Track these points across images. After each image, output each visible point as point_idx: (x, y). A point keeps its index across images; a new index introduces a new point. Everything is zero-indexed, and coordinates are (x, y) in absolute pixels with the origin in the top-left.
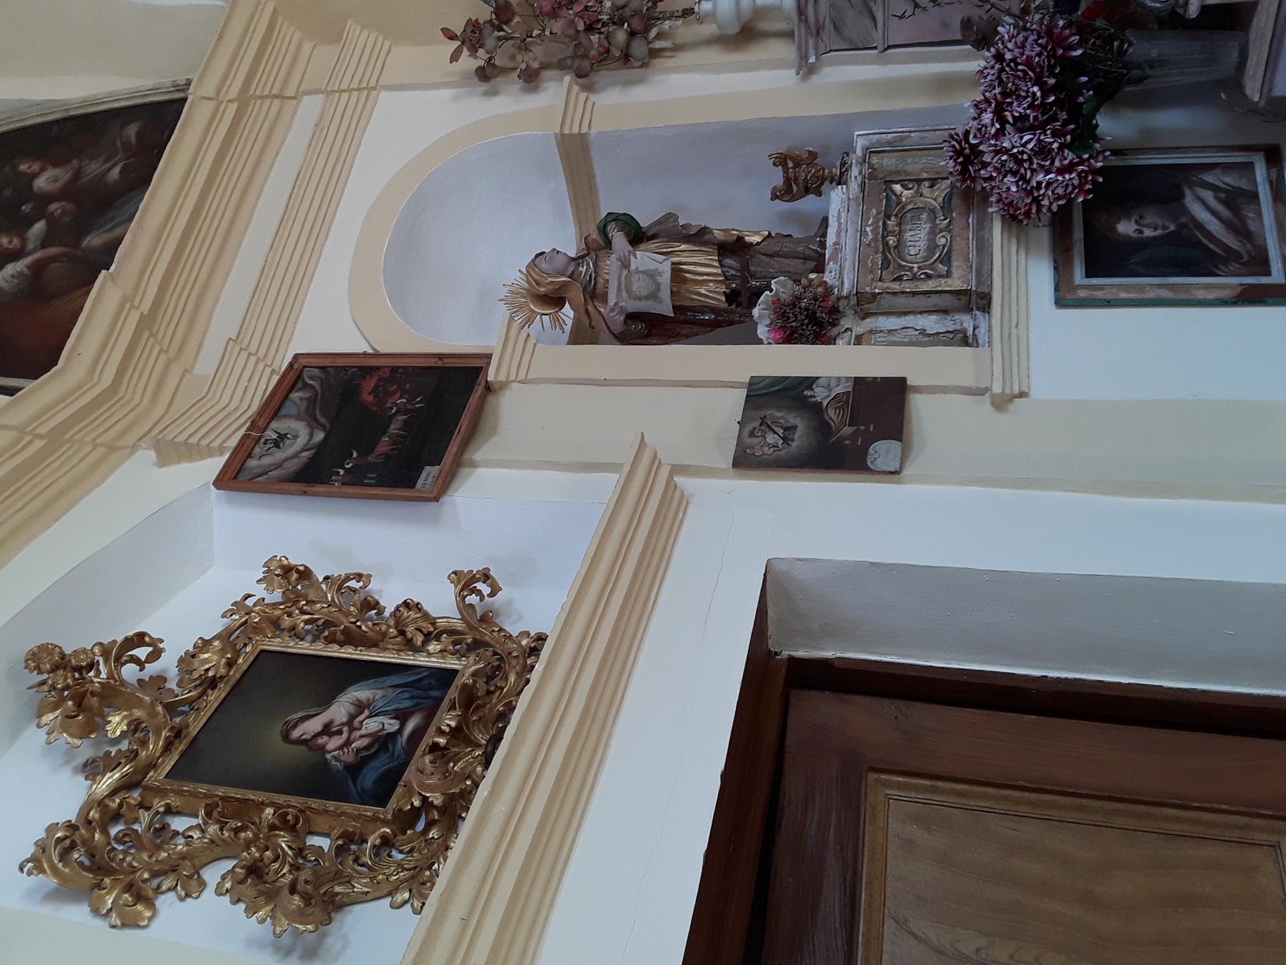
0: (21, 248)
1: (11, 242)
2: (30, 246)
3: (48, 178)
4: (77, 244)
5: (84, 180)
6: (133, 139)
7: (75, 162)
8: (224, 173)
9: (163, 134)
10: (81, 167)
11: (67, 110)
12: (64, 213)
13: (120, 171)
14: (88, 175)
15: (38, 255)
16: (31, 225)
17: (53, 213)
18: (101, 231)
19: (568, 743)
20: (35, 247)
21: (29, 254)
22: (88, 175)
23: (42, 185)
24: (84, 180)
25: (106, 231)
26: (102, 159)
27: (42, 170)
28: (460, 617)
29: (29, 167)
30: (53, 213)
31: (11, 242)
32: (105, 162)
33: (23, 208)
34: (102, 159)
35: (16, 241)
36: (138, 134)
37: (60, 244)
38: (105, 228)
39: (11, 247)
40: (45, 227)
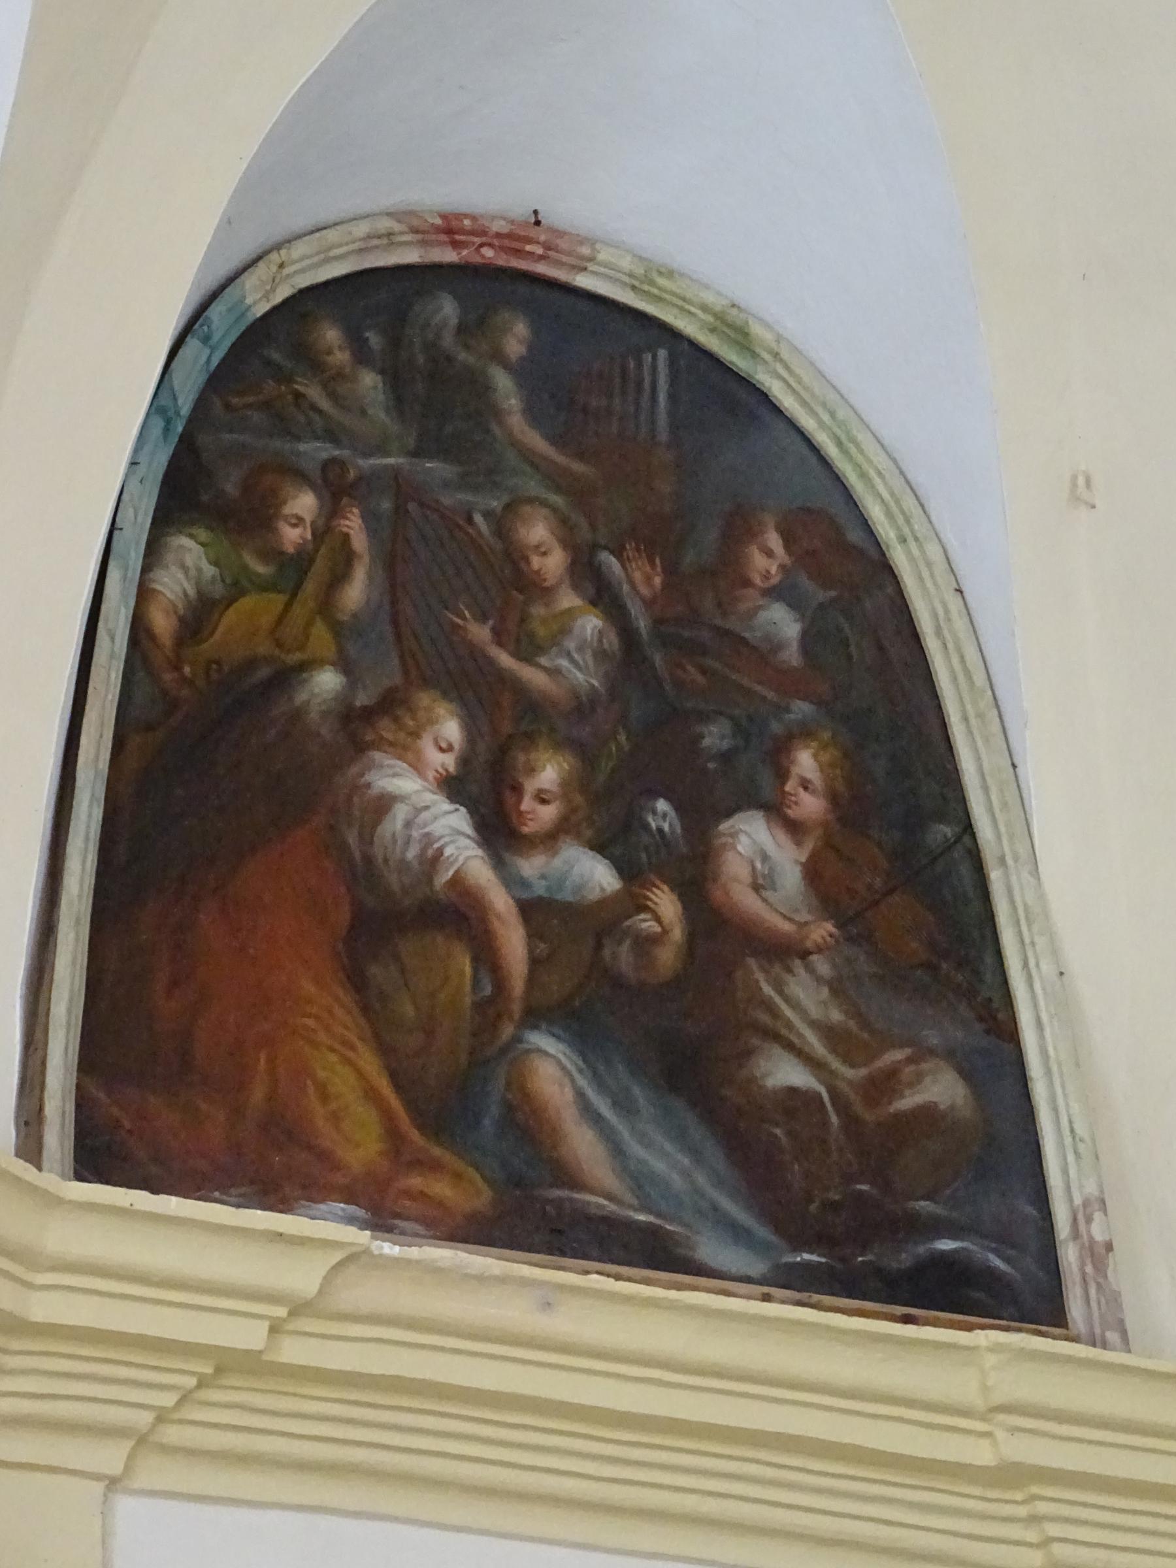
0: (524, 837)
1: (544, 801)
2: (530, 866)
3: (765, 857)
4: (534, 1016)
5: (760, 976)
6: (908, 1102)
7: (823, 931)
8: (758, 1462)
9: (927, 1197)
10: (804, 955)
11: (1002, 861)
12: (645, 944)
13: (793, 1091)
14: (779, 988)
15: (500, 901)
16: (600, 847)
17: (645, 908)
18: (582, 1082)
19: (26, 27)
20: (524, 884)
21: (499, 864)
22: (779, 988)
23: (743, 845)
24: (760, 976)
25: (580, 1095)
26: (836, 1016)
27: (795, 828)
28: (162, 623)
29: (805, 785)
30: (645, 908)
31: (542, 798)
32: (829, 1033)
33: (662, 805)
34: (836, 1016)
35: (548, 814)
36: (928, 1115)
37: (535, 962)
38: (591, 1093)
39: (527, 804)
40: (594, 895)
